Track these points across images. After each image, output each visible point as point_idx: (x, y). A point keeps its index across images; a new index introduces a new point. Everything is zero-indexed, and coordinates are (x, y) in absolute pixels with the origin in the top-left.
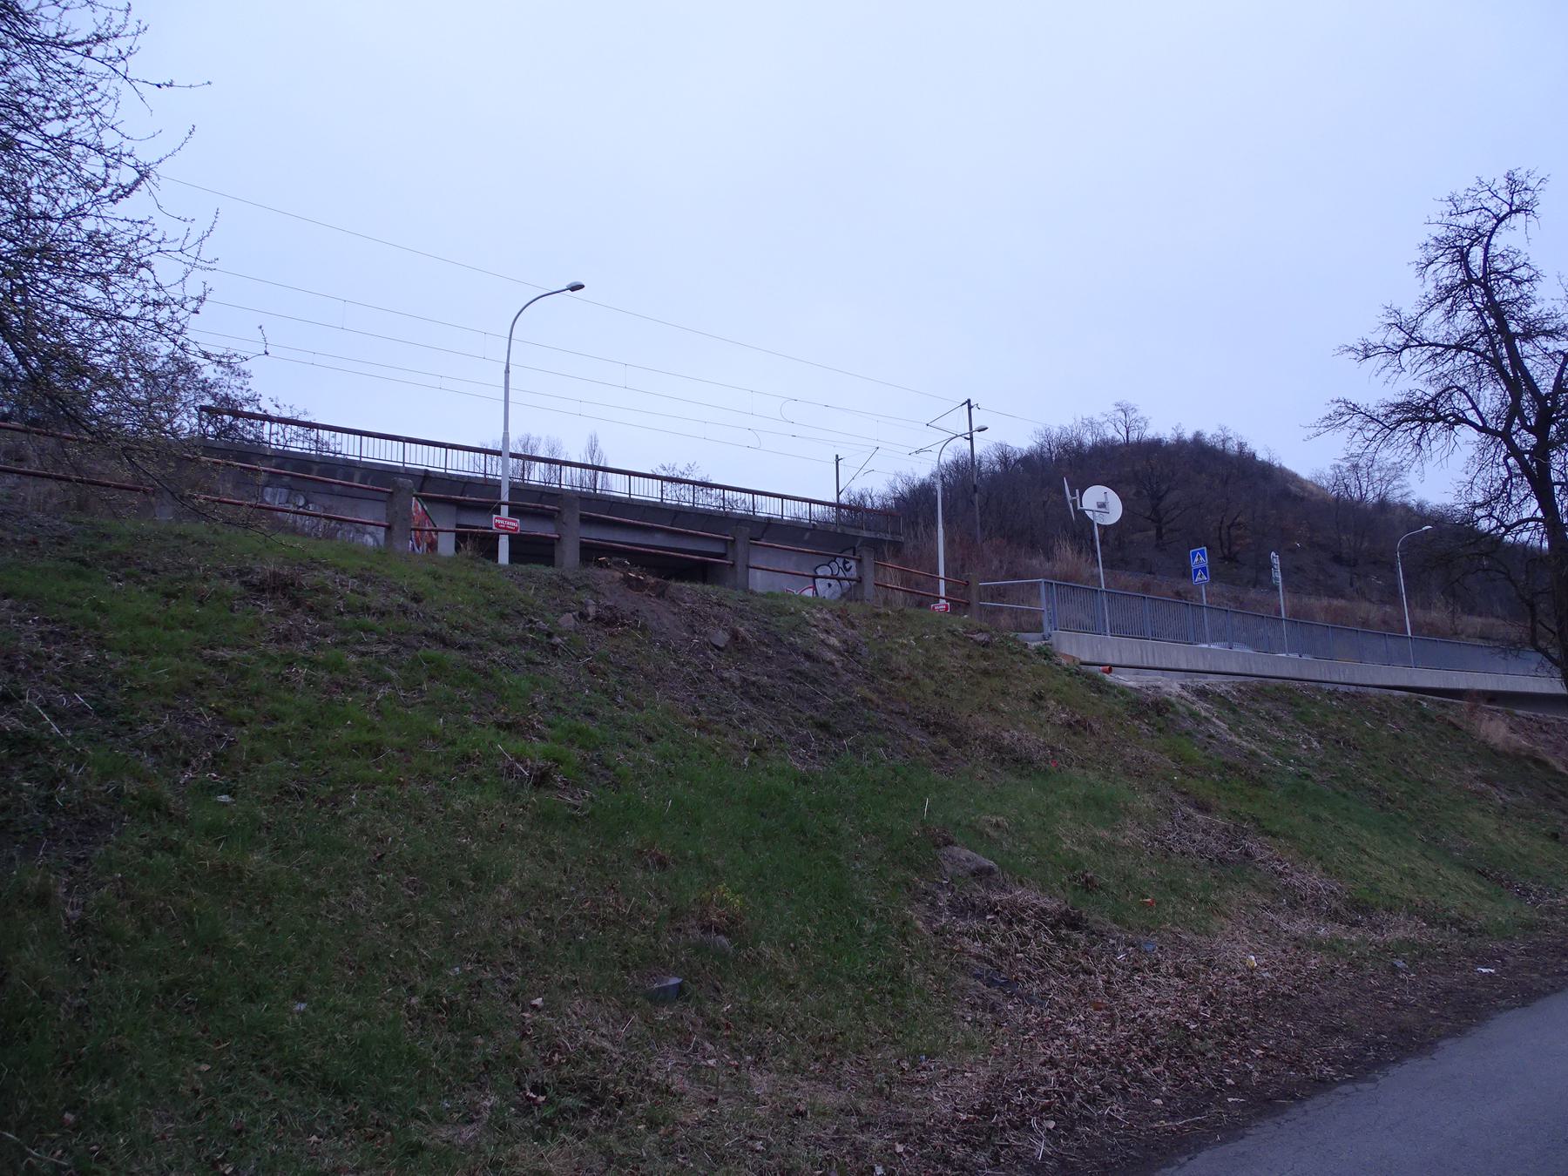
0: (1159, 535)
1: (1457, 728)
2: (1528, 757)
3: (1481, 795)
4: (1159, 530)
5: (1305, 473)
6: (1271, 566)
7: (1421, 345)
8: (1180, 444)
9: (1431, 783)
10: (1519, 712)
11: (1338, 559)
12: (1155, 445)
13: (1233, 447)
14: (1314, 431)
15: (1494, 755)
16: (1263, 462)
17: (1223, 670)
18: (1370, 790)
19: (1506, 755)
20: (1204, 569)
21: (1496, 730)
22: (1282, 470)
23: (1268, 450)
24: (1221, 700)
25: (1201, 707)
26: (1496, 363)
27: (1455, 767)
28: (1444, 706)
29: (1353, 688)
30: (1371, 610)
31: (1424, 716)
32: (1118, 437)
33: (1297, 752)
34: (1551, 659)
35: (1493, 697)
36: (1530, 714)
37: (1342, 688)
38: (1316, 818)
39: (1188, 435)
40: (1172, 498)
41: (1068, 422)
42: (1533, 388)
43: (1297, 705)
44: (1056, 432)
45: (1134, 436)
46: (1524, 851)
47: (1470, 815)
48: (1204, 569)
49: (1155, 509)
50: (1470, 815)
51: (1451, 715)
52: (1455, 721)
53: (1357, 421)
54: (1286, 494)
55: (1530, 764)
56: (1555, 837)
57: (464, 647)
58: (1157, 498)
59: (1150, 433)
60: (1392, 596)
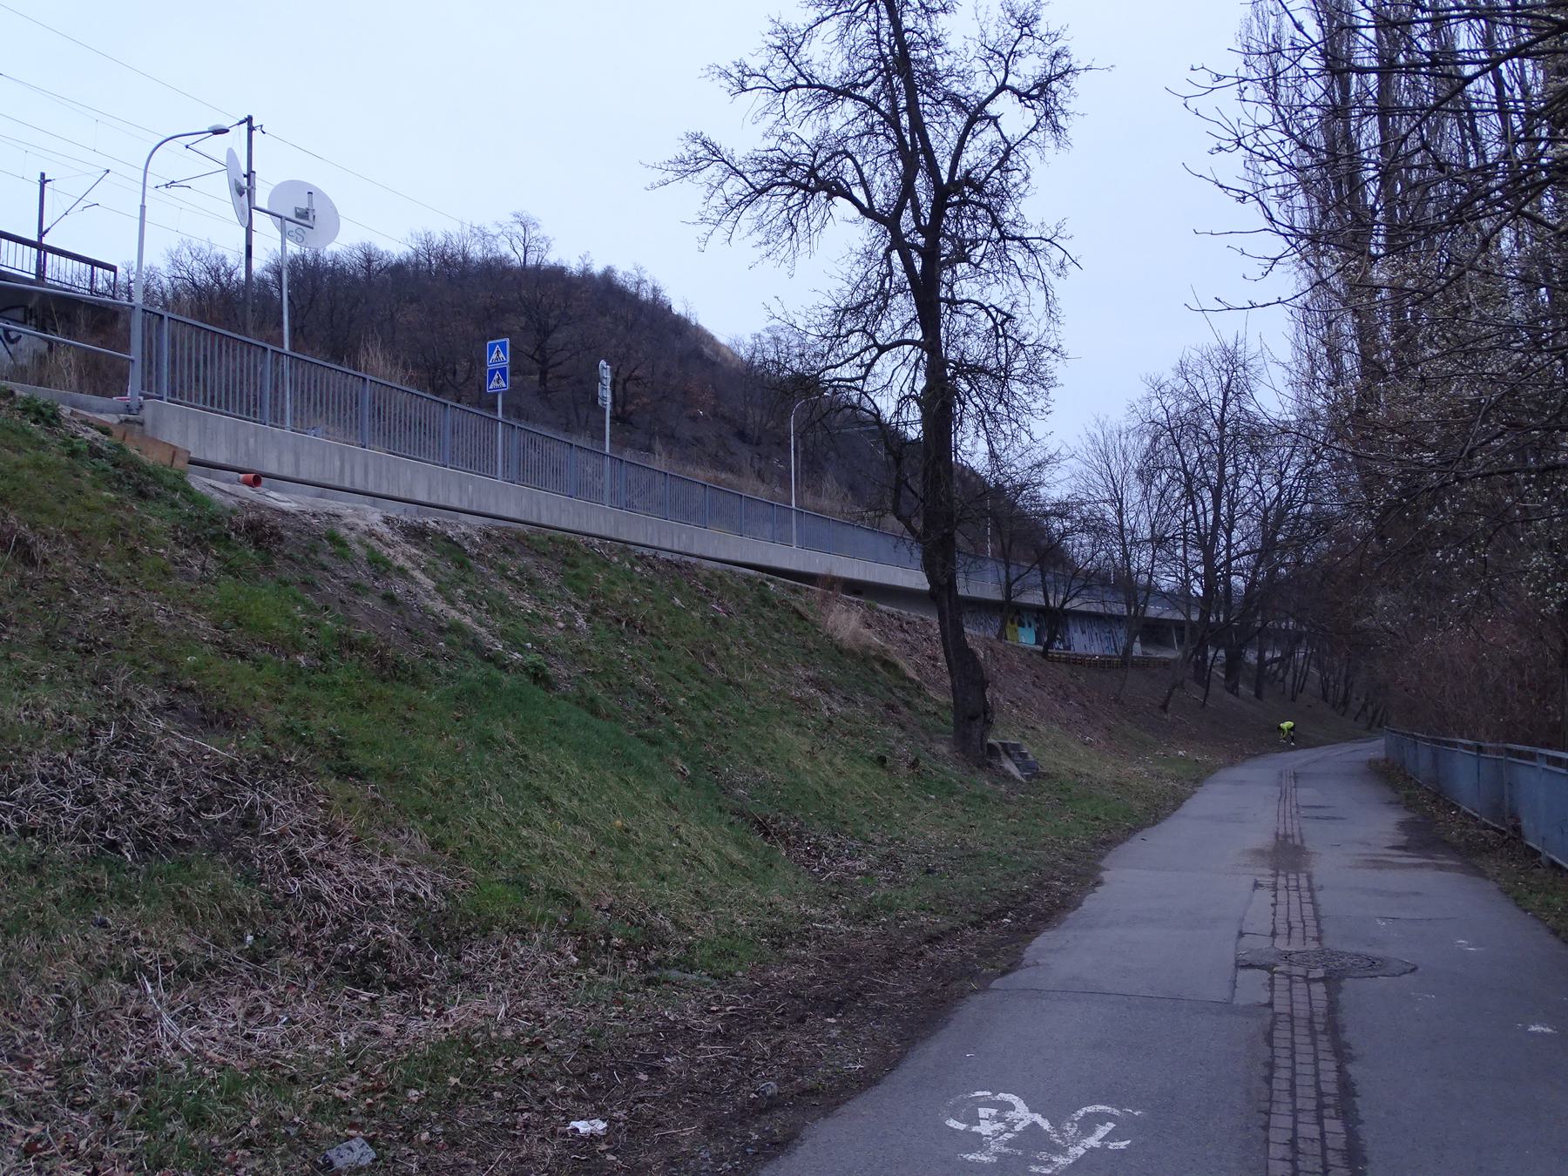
0: (543, 381)
1: (802, 617)
2: (877, 658)
3: (806, 704)
4: (543, 373)
5: (723, 338)
6: (599, 379)
7: (810, 86)
8: (586, 278)
9: (738, 686)
10: (884, 607)
11: (742, 435)
12: (558, 273)
13: (646, 295)
14: (658, 176)
15: (839, 653)
16: (678, 317)
17: (492, 511)
18: (640, 692)
19: (851, 653)
20: (502, 371)
21: (846, 622)
22: (698, 328)
23: (685, 302)
24: (452, 548)
25: (401, 554)
26: (892, 120)
27: (784, 666)
28: (795, 591)
29: (677, 557)
30: (763, 492)
31: (764, 600)
32: (513, 256)
33: (546, 633)
34: (913, 531)
35: (856, 588)
36: (894, 610)
37: (662, 555)
38: (486, 742)
39: (597, 269)
40: (559, 337)
41: (454, 228)
42: (933, 170)
43: (573, 565)
44: (438, 239)
45: (532, 260)
46: (836, 783)
47: (779, 732)
48: (502, 371)
49: (540, 348)
50: (779, 732)
51: (798, 603)
52: (801, 609)
53: (714, 171)
54: (699, 355)
55: (877, 667)
56: (882, 761)
57: (702, 681)
58: (545, 332)
59: (552, 258)
60: (784, 480)
